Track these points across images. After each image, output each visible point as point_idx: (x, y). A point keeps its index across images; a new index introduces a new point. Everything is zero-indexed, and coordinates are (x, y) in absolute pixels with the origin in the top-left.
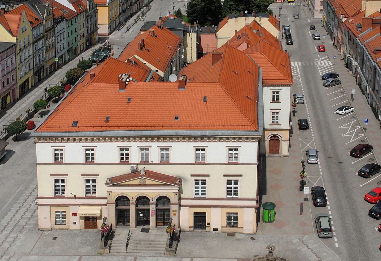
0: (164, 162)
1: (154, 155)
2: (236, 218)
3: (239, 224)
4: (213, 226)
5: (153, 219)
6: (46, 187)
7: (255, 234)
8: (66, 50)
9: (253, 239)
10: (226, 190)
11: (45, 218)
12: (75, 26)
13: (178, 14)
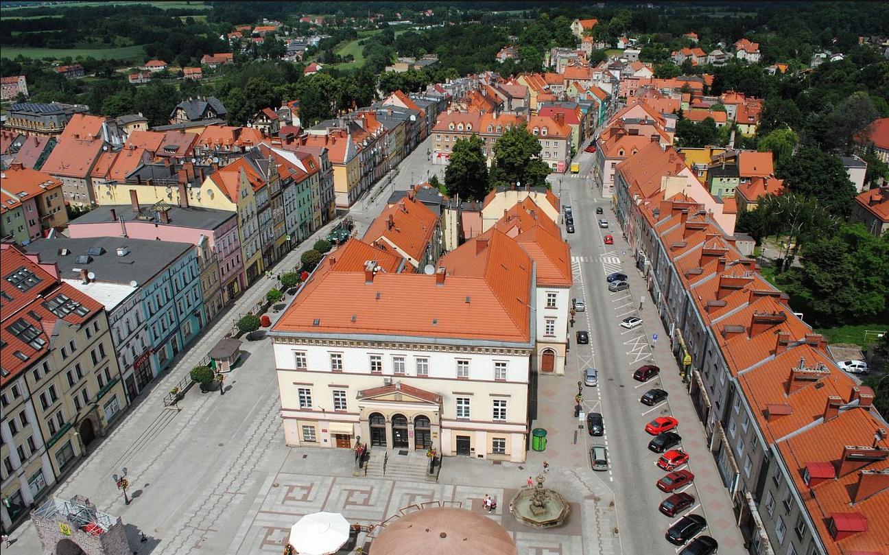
1: (411, 367)
2: (503, 445)
4: (477, 452)
5: (411, 441)
6: (290, 399)
9: (521, 468)
10: (493, 412)
12: (307, 192)
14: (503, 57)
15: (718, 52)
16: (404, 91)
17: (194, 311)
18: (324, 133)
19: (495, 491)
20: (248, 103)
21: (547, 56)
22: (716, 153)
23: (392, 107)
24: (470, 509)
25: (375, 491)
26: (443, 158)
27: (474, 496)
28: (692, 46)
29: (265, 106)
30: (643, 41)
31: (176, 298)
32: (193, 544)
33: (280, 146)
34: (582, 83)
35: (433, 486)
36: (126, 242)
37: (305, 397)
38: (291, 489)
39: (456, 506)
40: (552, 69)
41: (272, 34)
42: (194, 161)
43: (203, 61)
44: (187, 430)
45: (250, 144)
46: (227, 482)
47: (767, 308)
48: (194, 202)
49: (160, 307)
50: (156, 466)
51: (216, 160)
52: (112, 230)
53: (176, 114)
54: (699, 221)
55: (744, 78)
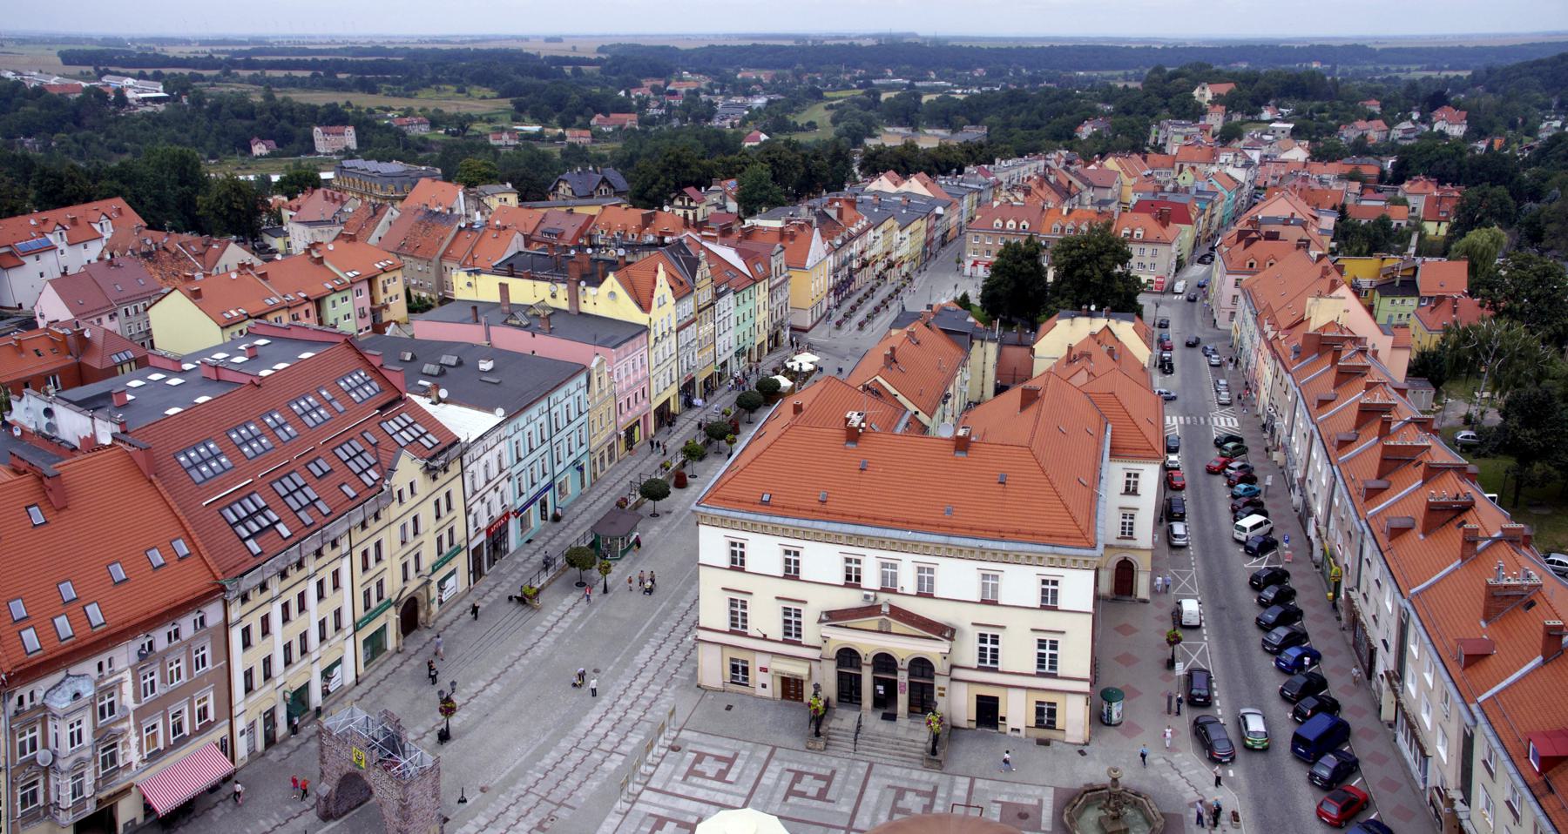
0: (925, 594)
1: (907, 580)
2: (1052, 713)
3: (1058, 725)
4: (1011, 723)
5: (903, 699)
6: (714, 612)
7: (1086, 744)
8: (732, 352)
9: (1082, 753)
10: (1035, 658)
11: (712, 668)
12: (750, 305)
13: (964, 302)
14: (1086, 131)
15: (1406, 125)
16: (929, 174)
17: (575, 462)
18: (778, 224)
19: (1038, 791)
20: (662, 179)
21: (1154, 129)
22: (1389, 263)
23: (877, 194)
24: (997, 819)
25: (838, 778)
26: (981, 268)
27: (1005, 798)
28: (1371, 117)
29: (689, 184)
30: (1299, 112)
31: (555, 440)
32: (536, 821)
33: (712, 239)
34: (1201, 168)
35: (936, 777)
36: (492, 352)
37: (738, 620)
38: (700, 757)
39: (974, 813)
40: (1159, 149)
41: (696, 92)
42: (589, 251)
43: (594, 122)
44: (550, 639)
45: (671, 234)
46: (600, 731)
47: (1448, 489)
48: (587, 308)
49: (531, 450)
50: (496, 687)
51: (621, 252)
52: (472, 334)
53: (556, 188)
54: (1358, 362)
55: (1440, 159)
